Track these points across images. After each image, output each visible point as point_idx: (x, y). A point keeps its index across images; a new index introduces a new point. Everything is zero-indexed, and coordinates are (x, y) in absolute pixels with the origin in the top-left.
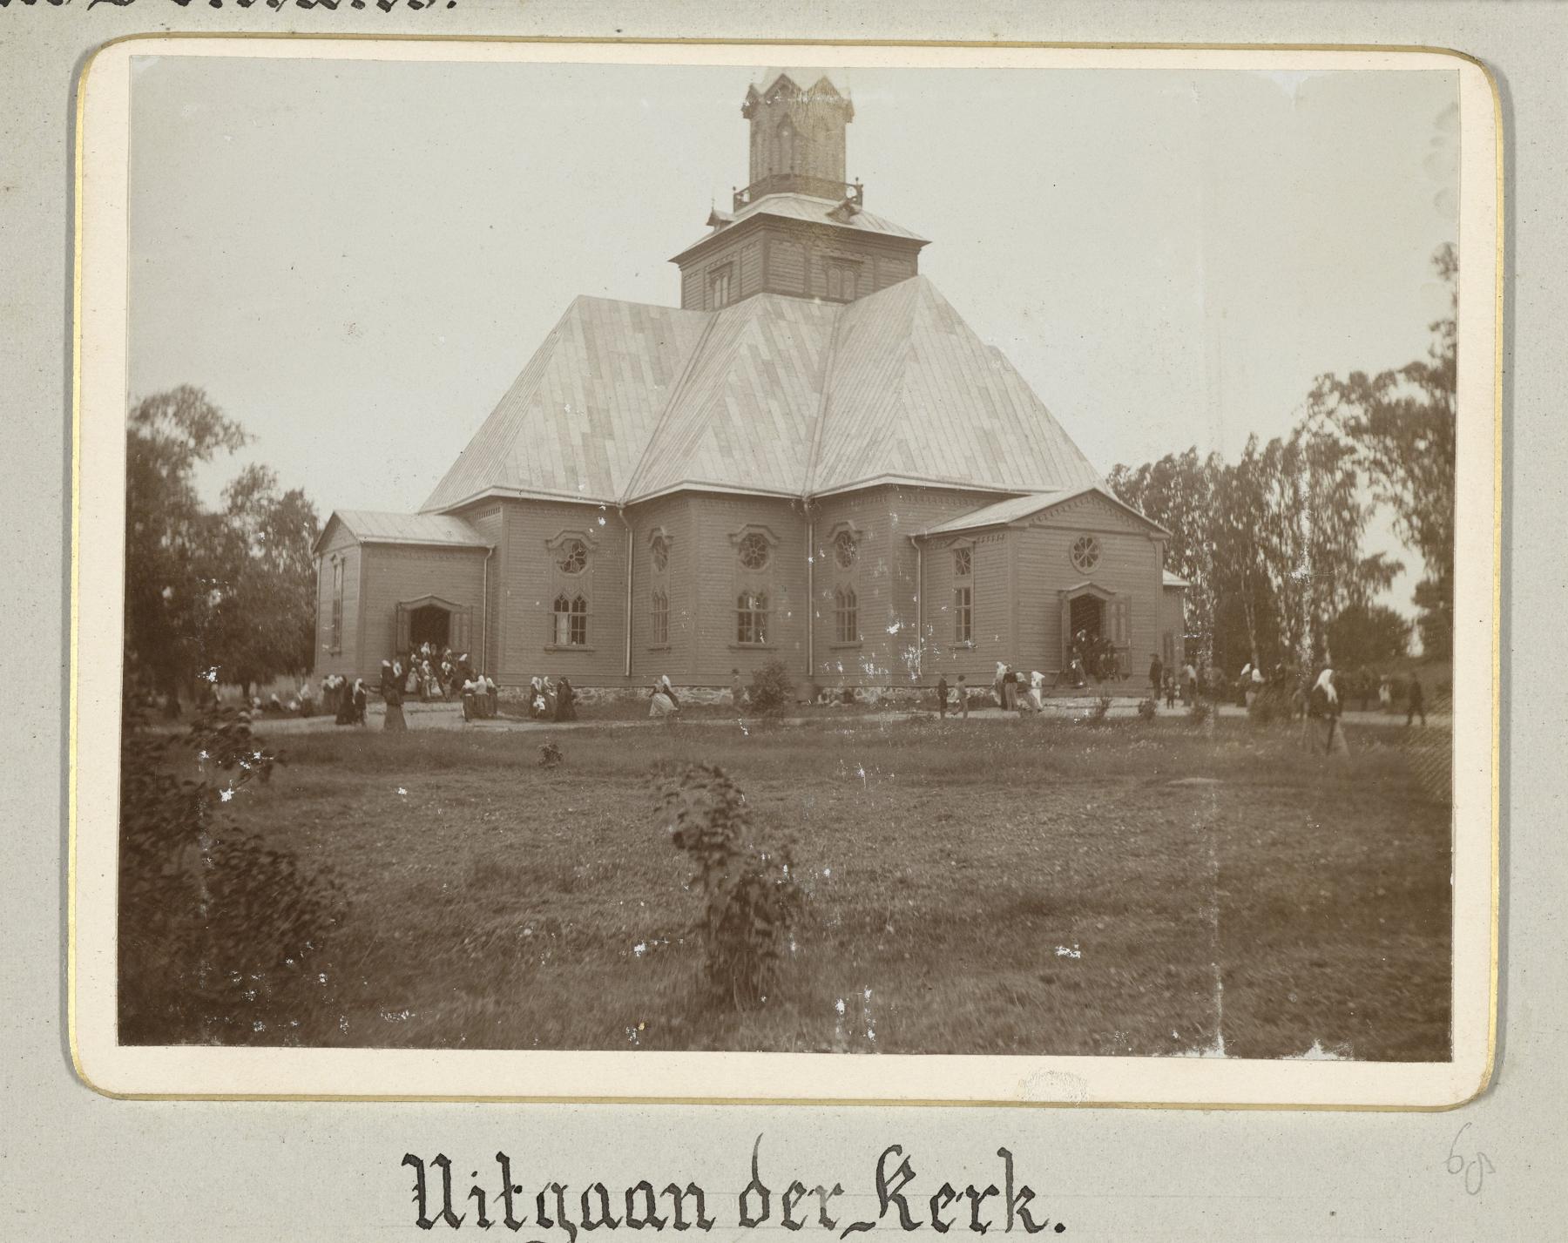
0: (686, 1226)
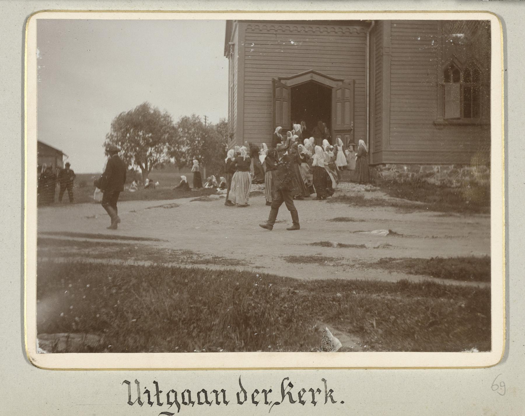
0: (202, 404)
